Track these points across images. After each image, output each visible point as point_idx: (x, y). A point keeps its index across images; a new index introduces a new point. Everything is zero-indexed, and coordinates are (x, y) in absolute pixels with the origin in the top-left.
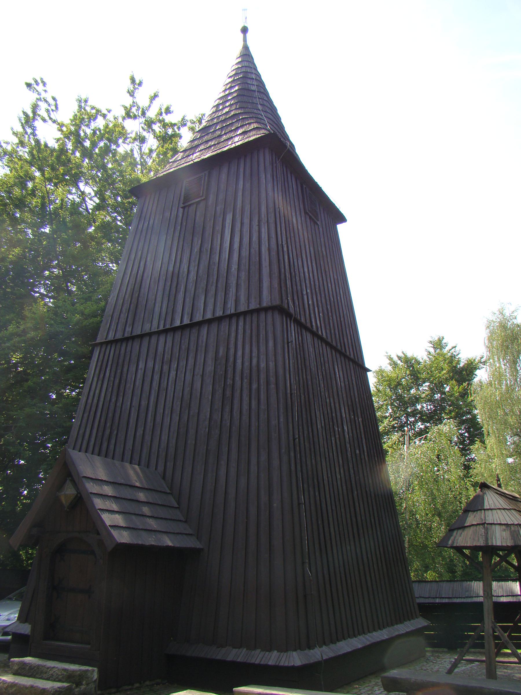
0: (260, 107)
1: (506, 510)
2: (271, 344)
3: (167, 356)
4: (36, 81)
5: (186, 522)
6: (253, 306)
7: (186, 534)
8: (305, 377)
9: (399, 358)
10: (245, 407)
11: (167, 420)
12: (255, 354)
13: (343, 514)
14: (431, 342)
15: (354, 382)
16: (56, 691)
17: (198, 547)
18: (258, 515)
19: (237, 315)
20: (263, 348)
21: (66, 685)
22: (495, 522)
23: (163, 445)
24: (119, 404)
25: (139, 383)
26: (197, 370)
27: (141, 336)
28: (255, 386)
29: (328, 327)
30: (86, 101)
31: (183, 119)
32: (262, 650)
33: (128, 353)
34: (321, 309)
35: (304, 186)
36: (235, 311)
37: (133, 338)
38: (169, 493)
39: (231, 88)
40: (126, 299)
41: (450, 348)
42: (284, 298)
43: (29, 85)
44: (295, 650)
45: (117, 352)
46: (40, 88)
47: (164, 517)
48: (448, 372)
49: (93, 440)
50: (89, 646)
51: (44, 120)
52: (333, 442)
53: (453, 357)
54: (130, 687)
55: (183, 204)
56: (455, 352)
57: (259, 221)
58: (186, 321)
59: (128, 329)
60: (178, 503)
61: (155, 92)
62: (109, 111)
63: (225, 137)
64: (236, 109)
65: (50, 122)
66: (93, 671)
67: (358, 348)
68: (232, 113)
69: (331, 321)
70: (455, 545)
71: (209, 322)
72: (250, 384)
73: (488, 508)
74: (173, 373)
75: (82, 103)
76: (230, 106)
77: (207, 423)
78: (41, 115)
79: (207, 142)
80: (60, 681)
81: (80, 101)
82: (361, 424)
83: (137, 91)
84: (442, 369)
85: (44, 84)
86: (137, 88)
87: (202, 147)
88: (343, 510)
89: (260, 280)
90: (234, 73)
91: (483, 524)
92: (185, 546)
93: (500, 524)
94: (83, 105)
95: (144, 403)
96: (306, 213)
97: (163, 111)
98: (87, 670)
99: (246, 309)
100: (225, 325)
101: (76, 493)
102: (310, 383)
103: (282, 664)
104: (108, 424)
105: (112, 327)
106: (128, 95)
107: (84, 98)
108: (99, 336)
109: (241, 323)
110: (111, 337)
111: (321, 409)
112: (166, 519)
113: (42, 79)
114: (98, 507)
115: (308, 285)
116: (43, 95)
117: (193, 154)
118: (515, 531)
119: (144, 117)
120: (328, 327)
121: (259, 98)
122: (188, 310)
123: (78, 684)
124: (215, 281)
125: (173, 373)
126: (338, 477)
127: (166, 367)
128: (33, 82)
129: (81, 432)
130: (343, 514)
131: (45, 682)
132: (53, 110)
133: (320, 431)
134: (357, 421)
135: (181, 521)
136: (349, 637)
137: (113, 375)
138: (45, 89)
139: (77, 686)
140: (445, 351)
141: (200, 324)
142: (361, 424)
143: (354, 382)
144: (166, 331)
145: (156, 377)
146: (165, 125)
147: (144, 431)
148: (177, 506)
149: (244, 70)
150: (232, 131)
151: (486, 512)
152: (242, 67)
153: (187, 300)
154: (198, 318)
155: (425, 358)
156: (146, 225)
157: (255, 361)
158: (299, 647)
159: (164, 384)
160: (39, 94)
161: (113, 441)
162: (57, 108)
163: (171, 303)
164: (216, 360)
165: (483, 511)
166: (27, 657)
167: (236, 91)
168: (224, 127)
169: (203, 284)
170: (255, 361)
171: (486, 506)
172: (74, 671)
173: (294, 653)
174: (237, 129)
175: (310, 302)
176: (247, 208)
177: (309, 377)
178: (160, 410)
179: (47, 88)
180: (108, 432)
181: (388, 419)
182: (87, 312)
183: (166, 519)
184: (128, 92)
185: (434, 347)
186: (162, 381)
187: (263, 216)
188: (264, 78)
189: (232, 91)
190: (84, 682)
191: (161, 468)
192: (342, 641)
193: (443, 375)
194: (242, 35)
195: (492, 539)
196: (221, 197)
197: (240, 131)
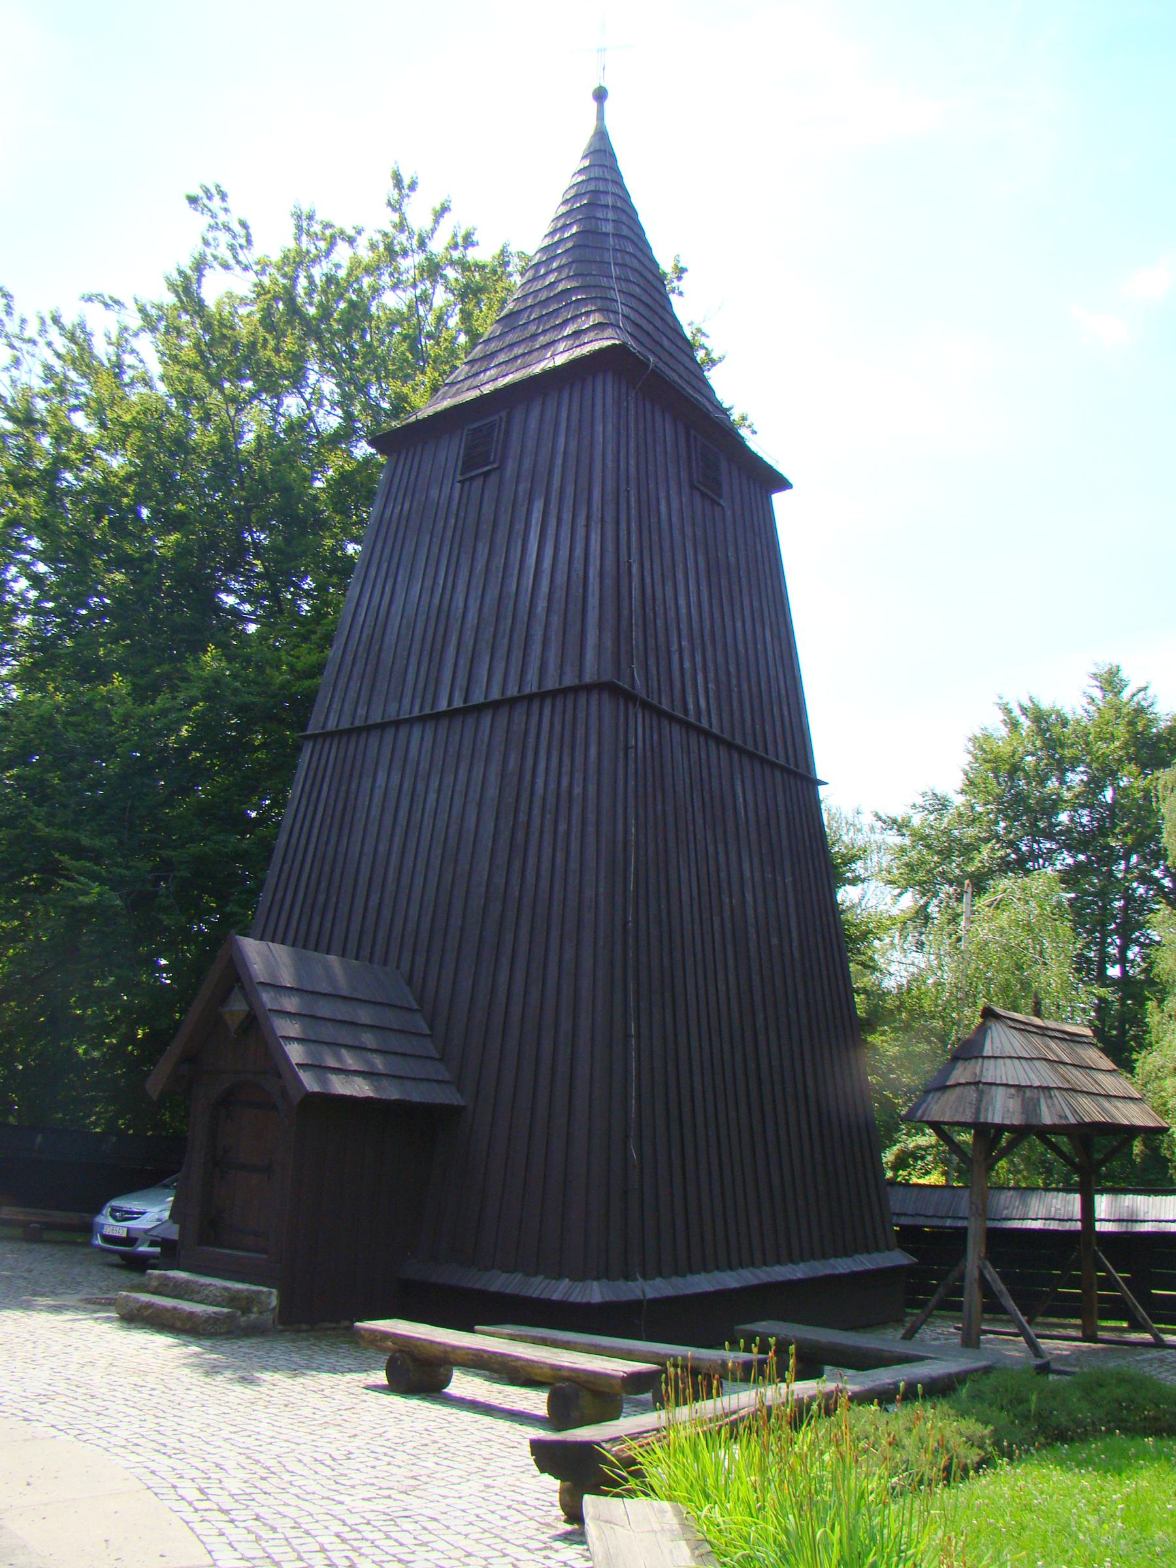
0: (615, 271)
1: (1023, 1061)
2: (593, 751)
3: (424, 766)
4: (207, 191)
5: (440, 1060)
6: (569, 680)
7: (438, 1081)
8: (659, 807)
9: (1024, 711)
10: (546, 865)
11: (419, 881)
12: (566, 769)
13: (727, 1057)
14: (1095, 676)
15: (781, 809)
16: (210, 1317)
17: (456, 1103)
18: (555, 1053)
19: (542, 696)
20: (579, 759)
21: (225, 1310)
22: (998, 1082)
23: (411, 925)
24: (342, 849)
25: (375, 812)
26: (471, 793)
27: (382, 726)
28: (562, 827)
29: (725, 708)
30: (310, 218)
31: (503, 252)
32: (546, 1278)
33: (359, 758)
34: (711, 676)
35: (693, 432)
36: (539, 688)
37: (368, 729)
38: (416, 1010)
39: (565, 227)
40: (359, 654)
41: (1134, 690)
42: (624, 666)
43: (193, 200)
44: (597, 1278)
45: (341, 755)
46: (216, 204)
47: (399, 1050)
48: (1125, 746)
49: (297, 910)
50: (264, 1256)
51: (226, 267)
52: (716, 926)
53: (1140, 711)
54: (333, 1325)
55: (462, 474)
56: (1144, 699)
57: (588, 518)
58: (458, 703)
59: (361, 712)
60: (431, 1027)
61: (443, 201)
62: (359, 233)
63: (542, 340)
64: (568, 277)
65: (237, 268)
66: (271, 1293)
67: (798, 741)
68: (560, 287)
69: (735, 696)
70: (925, 1119)
71: (495, 705)
72: (556, 822)
73: (990, 1054)
74: (432, 796)
75: (303, 221)
76: (560, 268)
77: (483, 889)
78: (219, 255)
79: (512, 346)
80: (217, 1305)
81: (299, 217)
82: (790, 889)
83: (406, 200)
84: (1113, 738)
85: (224, 197)
86: (408, 196)
87: (502, 358)
88: (726, 1047)
89: (583, 631)
90: (573, 192)
91: (976, 1083)
92: (430, 1101)
93: (1006, 1085)
94: (305, 224)
95: (382, 848)
96: (692, 486)
97: (460, 240)
98: (261, 1292)
99: (557, 686)
100: (520, 711)
101: (247, 1008)
102: (671, 819)
103: (571, 1299)
104: (323, 885)
105: (334, 706)
106: (389, 209)
107: (306, 210)
108: (312, 722)
109: (547, 711)
110: (331, 726)
111: (693, 866)
112: (404, 1055)
113: (218, 187)
114: (280, 1033)
115: (684, 632)
116: (222, 217)
117: (485, 371)
118: (1031, 1099)
119: (424, 251)
120: (725, 708)
121: (615, 250)
122: (461, 681)
123: (246, 1311)
124: (508, 631)
125: (432, 796)
126: (722, 987)
127: (421, 786)
128: (201, 194)
129: (279, 895)
130: (727, 1057)
131: (195, 1305)
132: (241, 247)
133: (686, 909)
134: (780, 884)
135: (432, 1058)
136: (718, 1269)
137: (333, 796)
138: (224, 205)
139: (243, 1313)
140: (1125, 695)
141: (479, 709)
142: (790, 889)
143: (781, 809)
144: (423, 719)
145: (405, 804)
146: (464, 266)
147: (381, 898)
148: (428, 1032)
149: (592, 187)
150: (554, 327)
151: (986, 1061)
152: (590, 179)
153: (461, 662)
154: (478, 698)
155: (1080, 712)
156: (397, 511)
157: (565, 783)
158: (604, 1274)
159: (417, 816)
160: (214, 216)
161: (330, 916)
162: (249, 242)
163: (434, 669)
164: (502, 777)
165: (980, 1060)
166: (173, 1269)
167: (572, 235)
168: (543, 316)
169: (487, 635)
170: (565, 783)
171: (987, 1051)
172: (238, 1291)
173: (595, 1283)
174: (565, 323)
175: (687, 665)
176: (570, 490)
177: (670, 809)
178: (409, 863)
179: (231, 203)
180: (322, 898)
181: (990, 845)
182: (300, 666)
183: (404, 1055)
184: (389, 204)
185: (1101, 688)
186: (414, 807)
187: (595, 508)
188: (637, 201)
189: (566, 235)
190: (255, 1309)
191: (406, 966)
192: (698, 1273)
193: (1114, 751)
194: (595, 105)
195: (987, 1110)
196: (527, 464)
197: (568, 331)
